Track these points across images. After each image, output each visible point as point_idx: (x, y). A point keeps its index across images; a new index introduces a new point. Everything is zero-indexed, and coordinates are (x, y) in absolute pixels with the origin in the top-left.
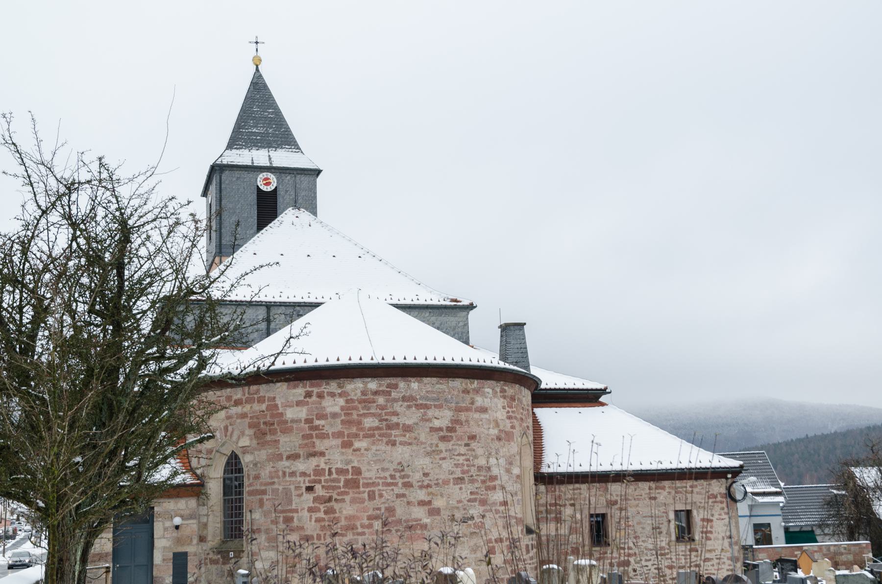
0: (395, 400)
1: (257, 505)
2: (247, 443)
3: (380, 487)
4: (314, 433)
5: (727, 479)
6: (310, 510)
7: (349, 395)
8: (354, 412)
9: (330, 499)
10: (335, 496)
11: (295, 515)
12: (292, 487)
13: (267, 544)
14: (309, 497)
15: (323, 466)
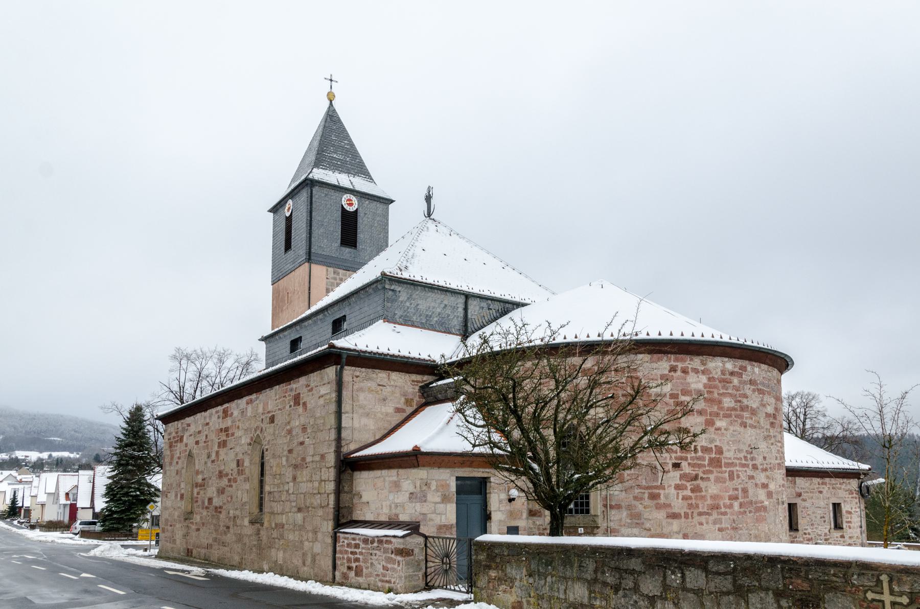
0: (745, 383)
3: (738, 468)
5: (859, 478)
6: (677, 487)
7: (711, 373)
8: (716, 391)
9: (696, 478)
10: (701, 475)
11: (662, 492)
14: (674, 477)
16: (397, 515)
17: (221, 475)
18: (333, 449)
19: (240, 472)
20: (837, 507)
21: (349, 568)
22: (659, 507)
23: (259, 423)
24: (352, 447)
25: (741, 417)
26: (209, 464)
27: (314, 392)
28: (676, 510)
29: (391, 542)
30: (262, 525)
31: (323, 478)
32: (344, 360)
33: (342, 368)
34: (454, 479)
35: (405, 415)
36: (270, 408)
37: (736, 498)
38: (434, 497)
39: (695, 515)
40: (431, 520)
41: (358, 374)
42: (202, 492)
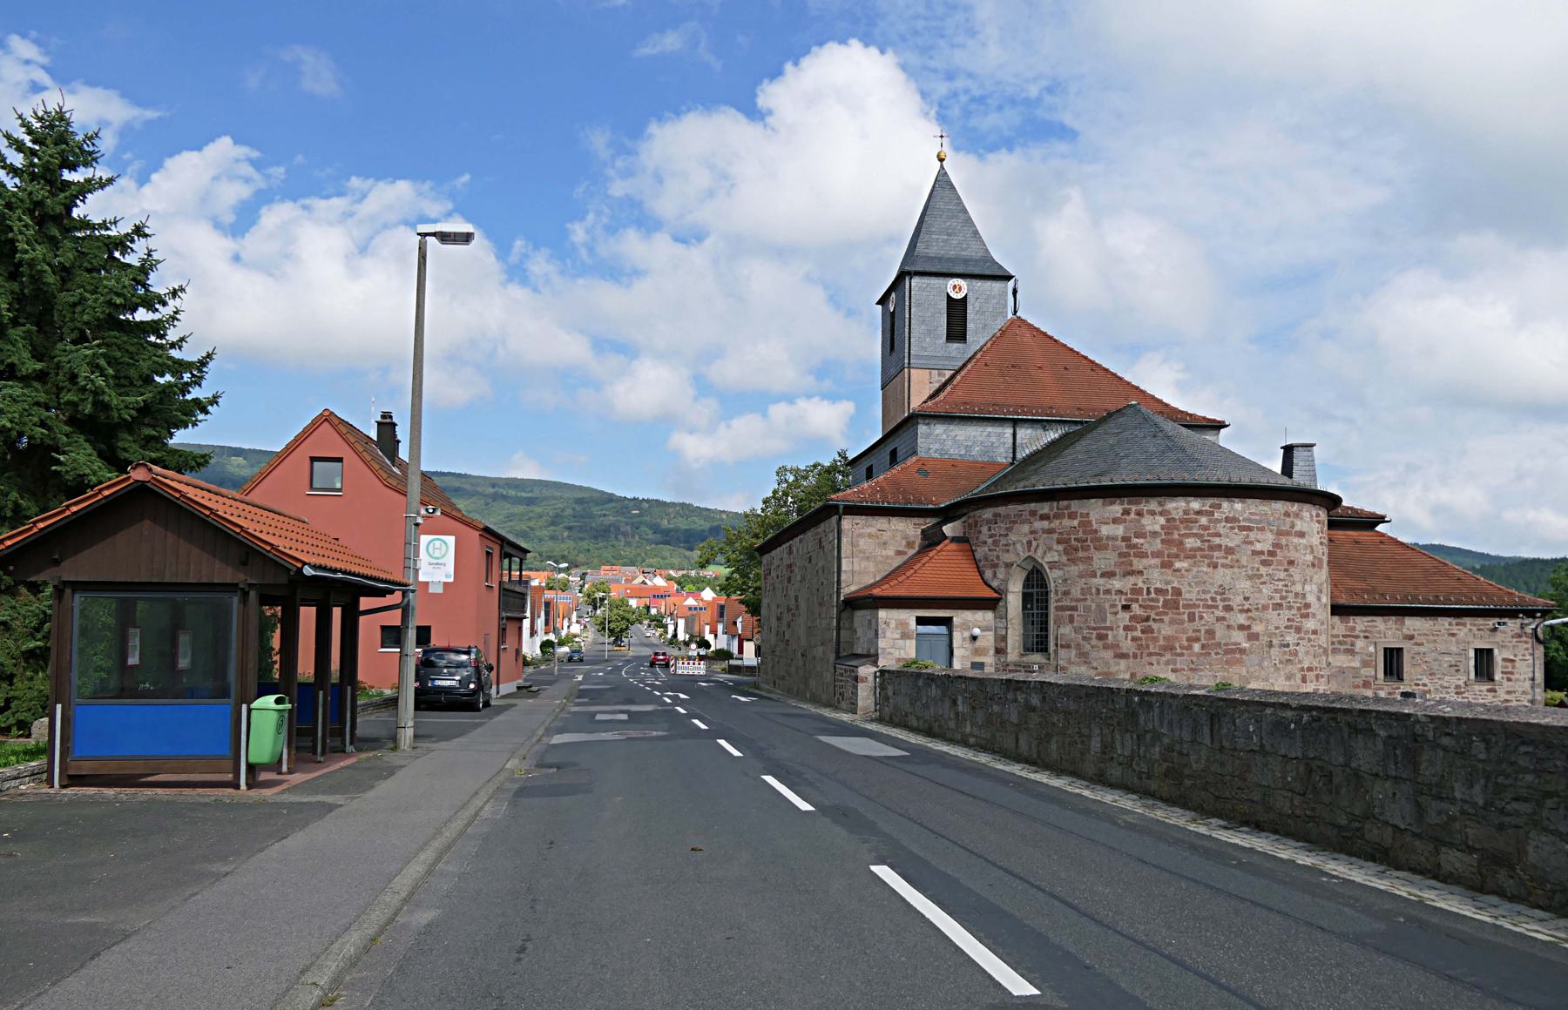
6: (1126, 628)
9: (1147, 619)
12: (1107, 606)
14: (1124, 617)
15: (1140, 585)
22: (1106, 647)
28: (1124, 651)
37: (1197, 640)
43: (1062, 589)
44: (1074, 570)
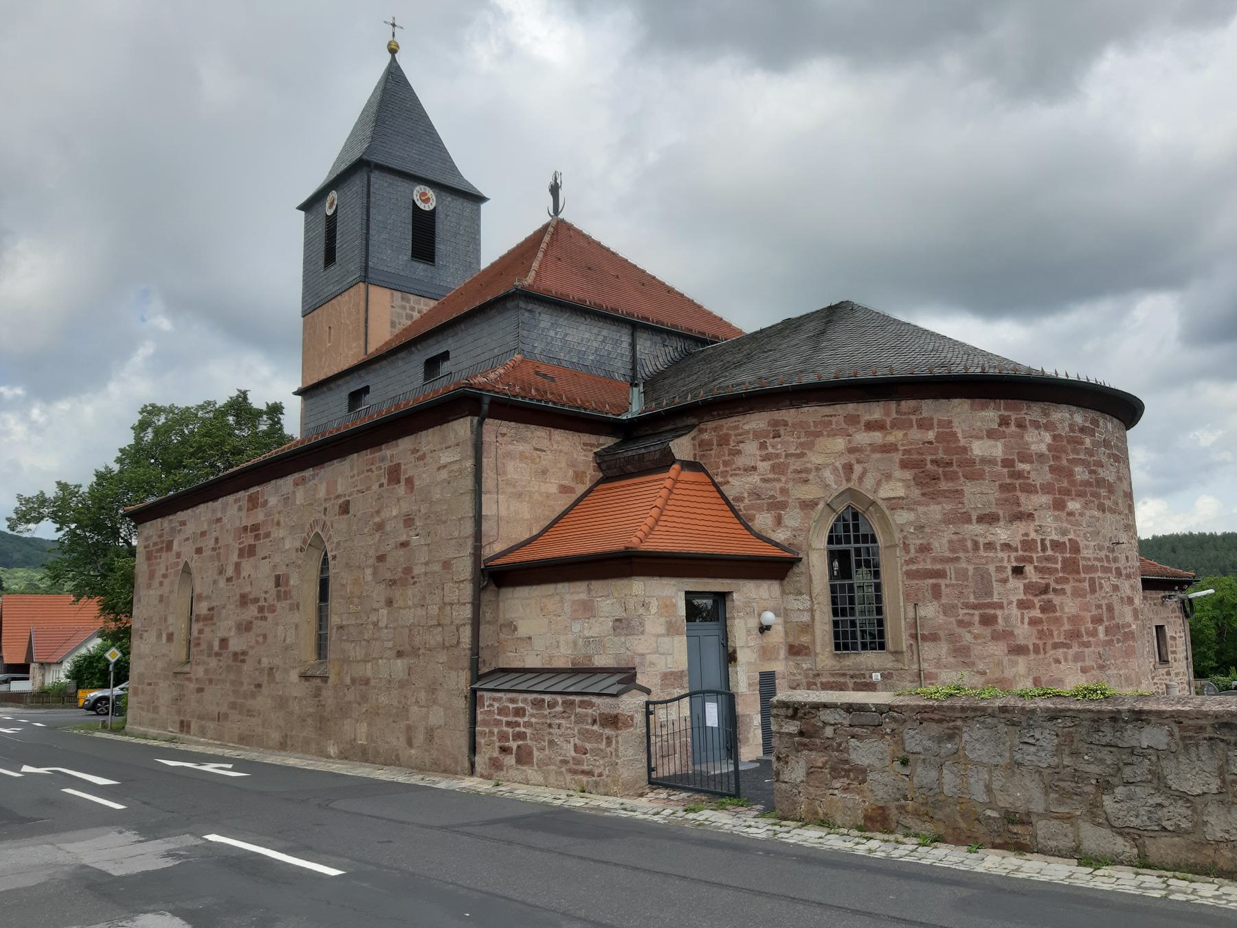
1: (928, 595)
2: (901, 492)
4: (1017, 483)
6: (1022, 605)
9: (1045, 590)
10: (1053, 585)
11: (999, 612)
12: (992, 568)
13: (952, 660)
14: (1016, 584)
15: (1033, 535)
16: (590, 658)
17: (244, 600)
18: (469, 549)
19: (283, 595)
20: (1160, 629)
21: (504, 750)
22: (996, 637)
23: (317, 516)
24: (498, 548)
25: (1096, 495)
26: (222, 583)
27: (428, 460)
29: (591, 705)
30: (325, 679)
31: (447, 600)
32: (486, 407)
33: (481, 423)
34: (683, 595)
35: (574, 497)
36: (340, 490)
38: (654, 625)
39: (1049, 647)
40: (652, 664)
41: (504, 430)
42: (207, 630)
43: (915, 542)
44: (935, 511)
